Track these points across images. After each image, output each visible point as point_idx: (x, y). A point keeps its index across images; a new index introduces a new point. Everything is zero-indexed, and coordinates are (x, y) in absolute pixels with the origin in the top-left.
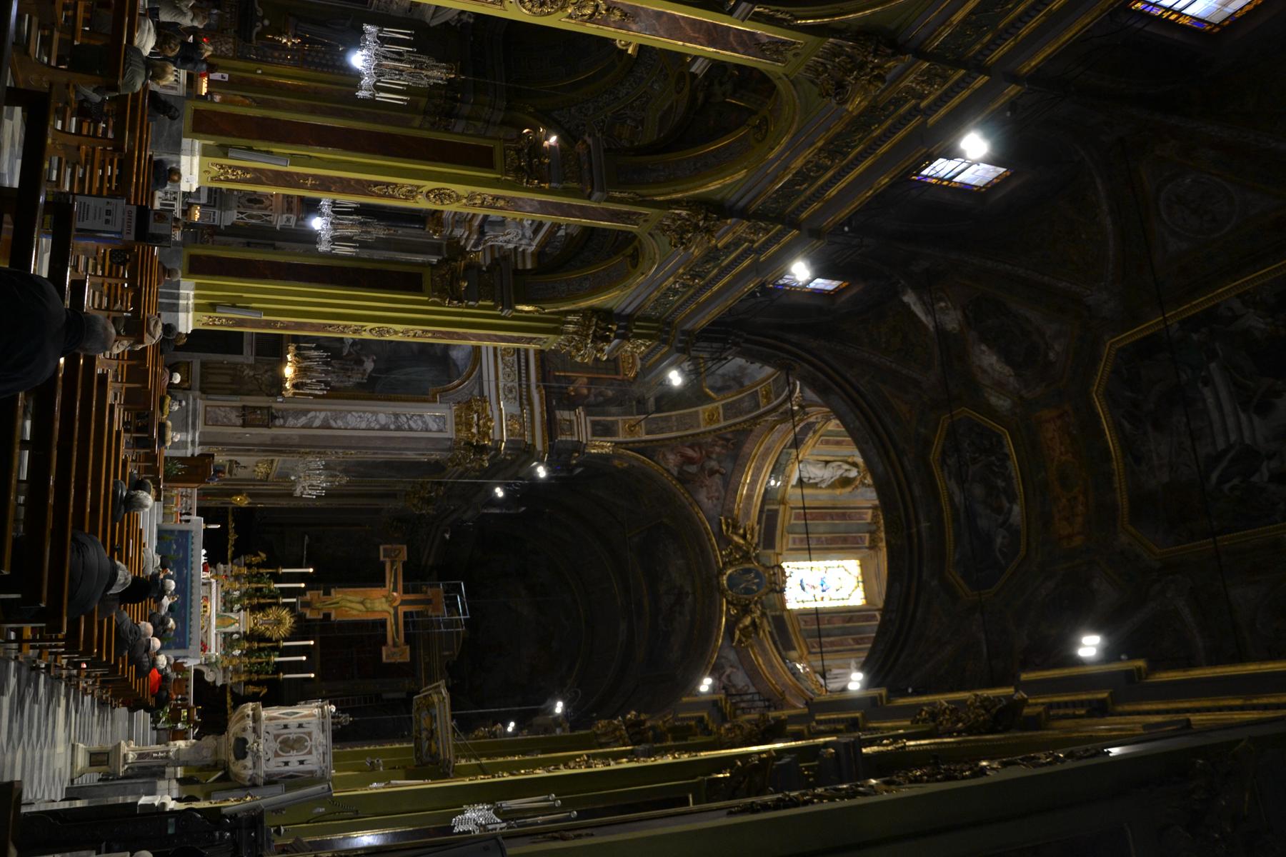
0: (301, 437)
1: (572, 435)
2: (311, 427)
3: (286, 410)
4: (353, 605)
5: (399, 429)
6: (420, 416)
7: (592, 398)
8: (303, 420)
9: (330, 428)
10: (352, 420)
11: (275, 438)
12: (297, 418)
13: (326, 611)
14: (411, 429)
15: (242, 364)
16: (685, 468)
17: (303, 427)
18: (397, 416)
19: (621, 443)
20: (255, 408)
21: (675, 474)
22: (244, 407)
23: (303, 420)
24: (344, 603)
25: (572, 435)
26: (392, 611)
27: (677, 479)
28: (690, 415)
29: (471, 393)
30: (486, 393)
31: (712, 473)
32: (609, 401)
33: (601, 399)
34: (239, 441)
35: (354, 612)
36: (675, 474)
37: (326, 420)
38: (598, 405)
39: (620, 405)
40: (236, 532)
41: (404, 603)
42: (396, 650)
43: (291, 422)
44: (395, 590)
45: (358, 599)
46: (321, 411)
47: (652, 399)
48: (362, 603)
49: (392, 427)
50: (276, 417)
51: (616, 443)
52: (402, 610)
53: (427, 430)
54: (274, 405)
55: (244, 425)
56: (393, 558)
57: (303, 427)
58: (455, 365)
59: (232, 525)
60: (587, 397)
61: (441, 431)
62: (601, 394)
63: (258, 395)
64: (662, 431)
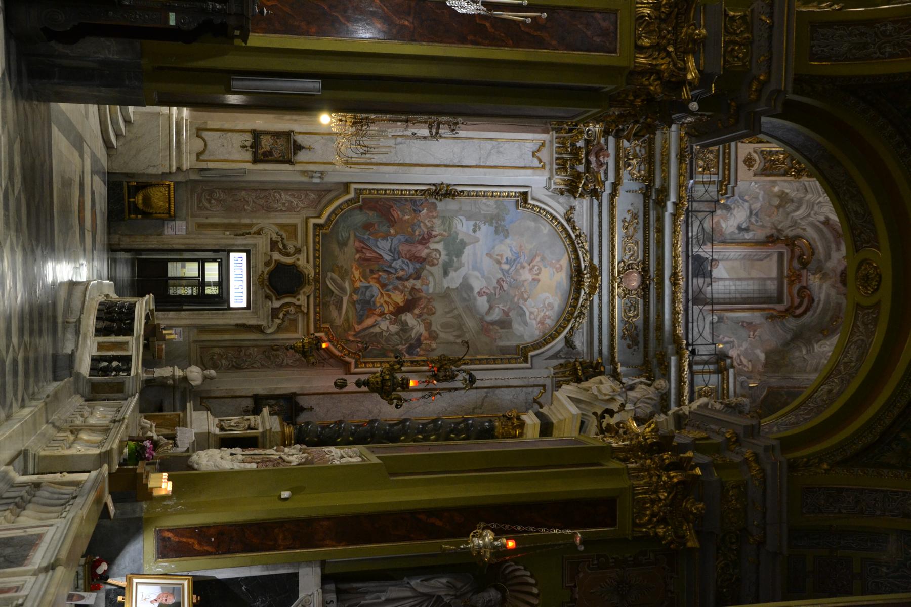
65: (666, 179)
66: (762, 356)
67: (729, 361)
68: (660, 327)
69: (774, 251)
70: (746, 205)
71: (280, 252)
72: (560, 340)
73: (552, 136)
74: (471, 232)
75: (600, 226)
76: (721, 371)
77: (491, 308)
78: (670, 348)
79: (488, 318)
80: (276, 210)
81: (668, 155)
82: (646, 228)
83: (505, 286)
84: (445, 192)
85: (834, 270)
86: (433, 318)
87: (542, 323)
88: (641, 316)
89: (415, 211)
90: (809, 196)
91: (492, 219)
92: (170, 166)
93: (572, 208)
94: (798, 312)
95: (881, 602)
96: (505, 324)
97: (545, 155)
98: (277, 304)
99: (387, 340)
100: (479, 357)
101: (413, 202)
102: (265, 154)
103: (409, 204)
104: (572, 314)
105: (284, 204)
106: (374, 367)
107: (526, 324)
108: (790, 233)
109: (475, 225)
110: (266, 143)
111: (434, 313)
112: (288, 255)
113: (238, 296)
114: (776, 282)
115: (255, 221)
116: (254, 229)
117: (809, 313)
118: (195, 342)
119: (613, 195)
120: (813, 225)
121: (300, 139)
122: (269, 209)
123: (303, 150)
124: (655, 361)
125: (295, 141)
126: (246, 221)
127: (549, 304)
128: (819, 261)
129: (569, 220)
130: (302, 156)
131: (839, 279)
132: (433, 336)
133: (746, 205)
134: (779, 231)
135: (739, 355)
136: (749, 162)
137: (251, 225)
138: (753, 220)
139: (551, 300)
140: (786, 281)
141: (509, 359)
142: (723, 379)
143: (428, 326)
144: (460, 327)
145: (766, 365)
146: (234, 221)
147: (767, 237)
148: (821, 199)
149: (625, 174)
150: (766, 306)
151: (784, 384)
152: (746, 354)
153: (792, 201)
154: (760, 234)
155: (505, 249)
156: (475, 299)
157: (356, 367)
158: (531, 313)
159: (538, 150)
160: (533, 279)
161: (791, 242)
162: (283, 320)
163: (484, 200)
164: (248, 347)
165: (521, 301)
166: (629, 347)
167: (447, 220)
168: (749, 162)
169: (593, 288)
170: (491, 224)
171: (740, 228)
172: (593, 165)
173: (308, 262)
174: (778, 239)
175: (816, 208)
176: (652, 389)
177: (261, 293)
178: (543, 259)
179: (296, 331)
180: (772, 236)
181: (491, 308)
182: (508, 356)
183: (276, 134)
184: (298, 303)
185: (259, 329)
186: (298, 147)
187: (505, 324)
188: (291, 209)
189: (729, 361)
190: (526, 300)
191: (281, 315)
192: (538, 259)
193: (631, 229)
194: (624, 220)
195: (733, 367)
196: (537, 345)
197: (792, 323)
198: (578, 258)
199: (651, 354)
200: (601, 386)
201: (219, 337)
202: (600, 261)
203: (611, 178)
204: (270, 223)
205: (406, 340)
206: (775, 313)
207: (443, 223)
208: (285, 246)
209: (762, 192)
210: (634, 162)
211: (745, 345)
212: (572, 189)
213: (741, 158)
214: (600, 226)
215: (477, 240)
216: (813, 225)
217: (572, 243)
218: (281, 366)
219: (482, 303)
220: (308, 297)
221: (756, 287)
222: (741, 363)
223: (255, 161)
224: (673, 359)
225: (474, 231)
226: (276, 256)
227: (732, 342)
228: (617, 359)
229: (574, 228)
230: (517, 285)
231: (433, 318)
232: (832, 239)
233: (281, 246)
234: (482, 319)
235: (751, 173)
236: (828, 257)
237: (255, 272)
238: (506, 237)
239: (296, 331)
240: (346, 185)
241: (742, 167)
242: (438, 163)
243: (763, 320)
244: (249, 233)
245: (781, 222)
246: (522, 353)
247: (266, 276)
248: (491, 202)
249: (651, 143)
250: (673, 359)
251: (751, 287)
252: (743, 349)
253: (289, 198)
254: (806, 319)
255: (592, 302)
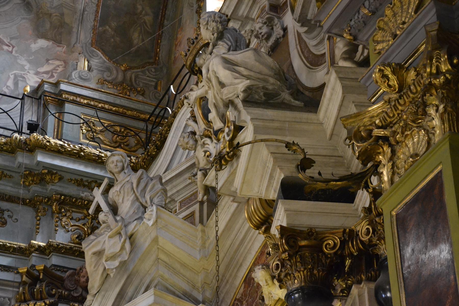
66: (42, 43)
67: (46, 87)
76: (60, 100)
78: (22, 159)
124: (35, 188)
135: (37, 73)
142: (73, 102)
145: (58, 41)
151: (90, 22)
176: (120, 177)
189: (46, 87)
195: (57, 85)
199: (22, 192)
200: (108, 252)
222: (50, 73)
224: (41, 158)
227: (16, 76)
228: (23, 245)
250: (41, 158)
252: (27, 66)
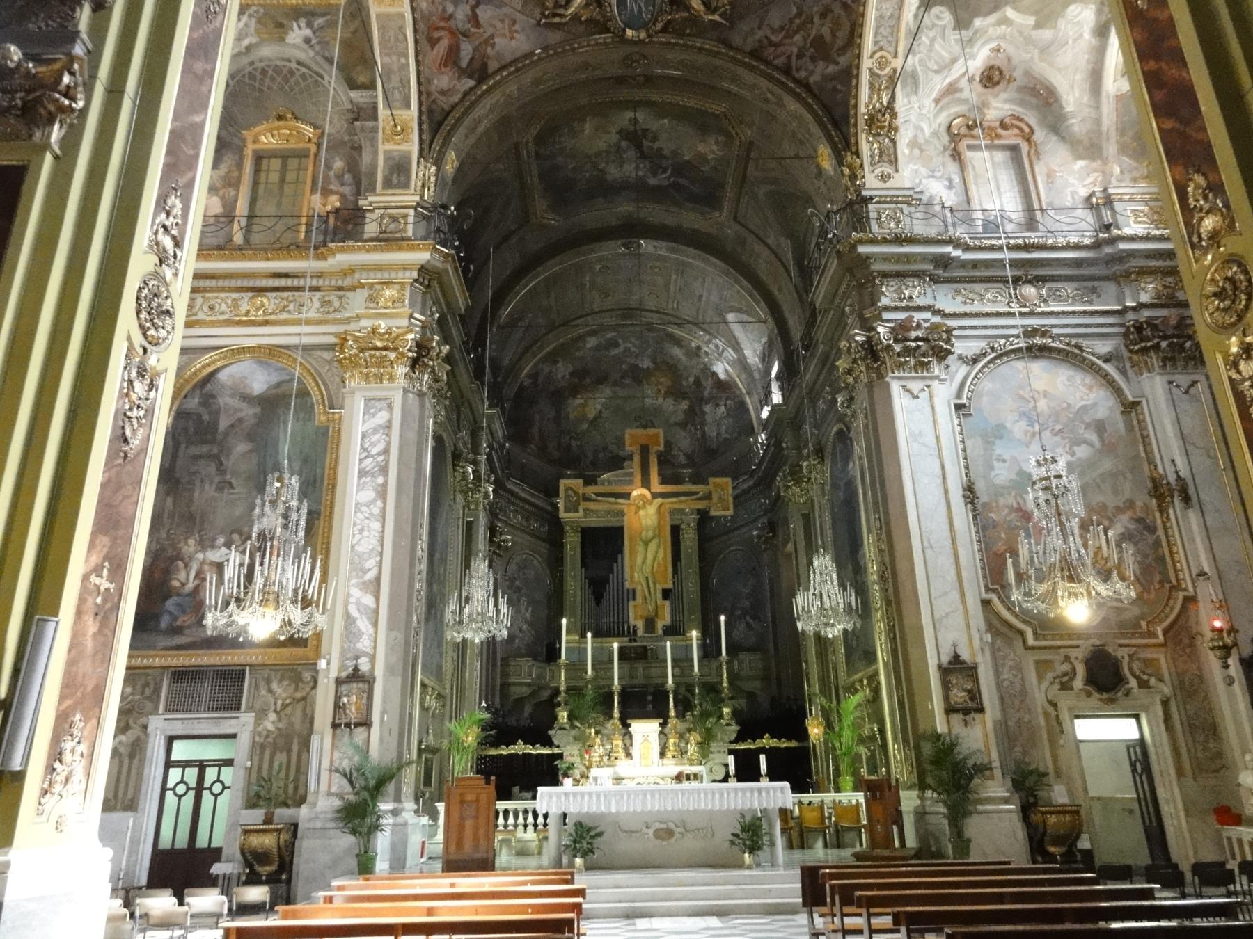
0: (391, 627)
1: (406, 216)
2: (376, 611)
3: (343, 652)
4: (650, 556)
5: (384, 470)
6: (364, 436)
7: (347, 190)
8: (363, 625)
9: (378, 579)
10: (367, 543)
11: (390, 670)
12: (359, 635)
13: (659, 595)
14: (386, 451)
15: (255, 733)
16: (464, 64)
17: (375, 624)
18: (362, 473)
19: (421, 150)
20: (338, 706)
21: (472, 83)
22: (335, 726)
23: (363, 625)
24: (648, 569)
25: (406, 216)
26: (659, 500)
27: (480, 82)
28: (382, 28)
29: (329, 362)
30: (332, 340)
31: (474, 20)
32: (353, 166)
33: (347, 177)
34: (395, 732)
35: (661, 555)
36: (472, 83)
37: (364, 586)
38: (358, 184)
39: (358, 149)
40: (762, 738)
41: (646, 483)
42: (715, 498)
43: (365, 644)
44: (627, 496)
45: (641, 548)
46: (348, 595)
47: (354, 94)
48: (646, 543)
49: (380, 480)
50: (356, 669)
51: (421, 155)
52: (657, 487)
53: (388, 426)
54: (334, 674)
55: (366, 724)
56: (577, 505)
57: (375, 624)
58: (278, 385)
59: (759, 743)
60: (343, 197)
61: (390, 407)
62: (340, 177)
63: (313, 704)
64: (405, 83)
65: (924, 258)
66: (1081, 163)
68: (1078, 263)
69: (968, 155)
70: (924, 181)
71: (1072, 679)
72: (1109, 368)
73: (894, 378)
74: (1006, 465)
75: (985, 327)
77: (1085, 442)
78: (1108, 250)
79: (1097, 444)
80: (1023, 685)
81: (899, 255)
82: (971, 280)
83: (1058, 427)
84: (970, 493)
85: (979, 95)
86: (1111, 505)
87: (1090, 388)
88: (1065, 284)
89: (994, 527)
90: (913, 118)
91: (988, 442)
92: (1010, 811)
93: (960, 357)
94: (1027, 130)
95: (711, 258)
96: (1100, 427)
97: (915, 386)
98: (1133, 683)
99: (1146, 556)
100: (1143, 454)
101: (984, 528)
102: (972, 699)
103: (987, 533)
104: (1076, 355)
105: (1015, 676)
106: (1181, 570)
107: (1095, 405)
108: (946, 139)
109: (998, 460)
110: (959, 696)
111: (1104, 505)
112: (1074, 670)
113: (1123, 729)
114: (995, 153)
115: (1040, 710)
116: (1050, 709)
117: (1026, 119)
118: (1195, 779)
119: (945, 315)
120: (936, 116)
121: (945, 659)
122: (1024, 692)
123: (959, 652)
125: (950, 663)
126: (1042, 721)
127: (1069, 380)
128: (969, 110)
129: (975, 361)
130: (965, 655)
131: (990, 90)
132: (1130, 504)
133: (924, 181)
134: (945, 149)
136: (884, 178)
137: (1046, 714)
138: (938, 174)
139: (1064, 378)
140: (997, 142)
141: (1139, 422)
143: (1119, 510)
144: (1114, 475)
145: (1093, 159)
146: (1045, 736)
147: (954, 160)
148: (916, 106)
149: (922, 302)
150: (1026, 161)
152: (1081, 179)
153: (916, 136)
154: (952, 168)
155: (1019, 428)
156: (1079, 459)
157: (1185, 590)
158: (1082, 399)
159: (911, 393)
160: (1045, 396)
161: (955, 138)
162: (1150, 675)
163: (968, 451)
164: (1188, 717)
165: (1072, 410)
166: (1099, 296)
167: (998, 491)
168: (884, 178)
169: (1044, 334)
170: (994, 444)
171: (950, 187)
172: (920, 334)
173: (1078, 647)
174: (955, 149)
175: (924, 112)
177: (1125, 702)
178: (1022, 388)
179: (1157, 660)
180: (952, 156)
181: (1085, 442)
182: (1135, 423)
183: (946, 687)
184: (1127, 658)
185: (1165, 703)
186: (956, 657)
187: (1100, 427)
188: (1018, 668)
190: (1069, 405)
191: (1145, 677)
192: (1021, 392)
193: (971, 296)
194: (965, 303)
196: (1118, 391)
197: (1039, 135)
198: (1014, 351)
201: (1184, 751)
202: (1013, 327)
203: (927, 315)
204: (1039, 692)
205: (1142, 534)
206: (1033, 151)
207: (1002, 495)
208: (1065, 674)
209: (911, 166)
210: (907, 293)
211: (1072, 180)
212: (942, 355)
213: (880, 185)
214: (985, 327)
215: (1014, 459)
216: (936, 116)
217: (999, 357)
218: (1201, 677)
219: (1082, 452)
220: (1120, 646)
221: (1003, 171)
223: (981, 710)
224: (1123, 246)
225: (1004, 461)
226: (1078, 683)
229: (984, 355)
230: (1055, 415)
231: (1111, 505)
232: (951, 97)
233: (1065, 679)
234: (1100, 451)
235: (896, 175)
236: (966, 101)
237: (1099, 709)
238: (1005, 427)
239: (1157, 660)
240: (986, 603)
241: (888, 185)
242: (943, 501)
243: (1042, 163)
244: (1057, 716)
245: (936, 148)
246: (1130, 407)
247: (1105, 696)
248: (968, 443)
249: (885, 275)
251: (1005, 177)
252: (1076, 182)
253: (1006, 670)
254: (1032, 121)
255: (1063, 335)
